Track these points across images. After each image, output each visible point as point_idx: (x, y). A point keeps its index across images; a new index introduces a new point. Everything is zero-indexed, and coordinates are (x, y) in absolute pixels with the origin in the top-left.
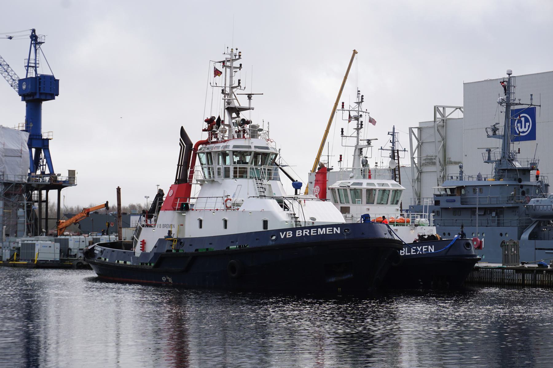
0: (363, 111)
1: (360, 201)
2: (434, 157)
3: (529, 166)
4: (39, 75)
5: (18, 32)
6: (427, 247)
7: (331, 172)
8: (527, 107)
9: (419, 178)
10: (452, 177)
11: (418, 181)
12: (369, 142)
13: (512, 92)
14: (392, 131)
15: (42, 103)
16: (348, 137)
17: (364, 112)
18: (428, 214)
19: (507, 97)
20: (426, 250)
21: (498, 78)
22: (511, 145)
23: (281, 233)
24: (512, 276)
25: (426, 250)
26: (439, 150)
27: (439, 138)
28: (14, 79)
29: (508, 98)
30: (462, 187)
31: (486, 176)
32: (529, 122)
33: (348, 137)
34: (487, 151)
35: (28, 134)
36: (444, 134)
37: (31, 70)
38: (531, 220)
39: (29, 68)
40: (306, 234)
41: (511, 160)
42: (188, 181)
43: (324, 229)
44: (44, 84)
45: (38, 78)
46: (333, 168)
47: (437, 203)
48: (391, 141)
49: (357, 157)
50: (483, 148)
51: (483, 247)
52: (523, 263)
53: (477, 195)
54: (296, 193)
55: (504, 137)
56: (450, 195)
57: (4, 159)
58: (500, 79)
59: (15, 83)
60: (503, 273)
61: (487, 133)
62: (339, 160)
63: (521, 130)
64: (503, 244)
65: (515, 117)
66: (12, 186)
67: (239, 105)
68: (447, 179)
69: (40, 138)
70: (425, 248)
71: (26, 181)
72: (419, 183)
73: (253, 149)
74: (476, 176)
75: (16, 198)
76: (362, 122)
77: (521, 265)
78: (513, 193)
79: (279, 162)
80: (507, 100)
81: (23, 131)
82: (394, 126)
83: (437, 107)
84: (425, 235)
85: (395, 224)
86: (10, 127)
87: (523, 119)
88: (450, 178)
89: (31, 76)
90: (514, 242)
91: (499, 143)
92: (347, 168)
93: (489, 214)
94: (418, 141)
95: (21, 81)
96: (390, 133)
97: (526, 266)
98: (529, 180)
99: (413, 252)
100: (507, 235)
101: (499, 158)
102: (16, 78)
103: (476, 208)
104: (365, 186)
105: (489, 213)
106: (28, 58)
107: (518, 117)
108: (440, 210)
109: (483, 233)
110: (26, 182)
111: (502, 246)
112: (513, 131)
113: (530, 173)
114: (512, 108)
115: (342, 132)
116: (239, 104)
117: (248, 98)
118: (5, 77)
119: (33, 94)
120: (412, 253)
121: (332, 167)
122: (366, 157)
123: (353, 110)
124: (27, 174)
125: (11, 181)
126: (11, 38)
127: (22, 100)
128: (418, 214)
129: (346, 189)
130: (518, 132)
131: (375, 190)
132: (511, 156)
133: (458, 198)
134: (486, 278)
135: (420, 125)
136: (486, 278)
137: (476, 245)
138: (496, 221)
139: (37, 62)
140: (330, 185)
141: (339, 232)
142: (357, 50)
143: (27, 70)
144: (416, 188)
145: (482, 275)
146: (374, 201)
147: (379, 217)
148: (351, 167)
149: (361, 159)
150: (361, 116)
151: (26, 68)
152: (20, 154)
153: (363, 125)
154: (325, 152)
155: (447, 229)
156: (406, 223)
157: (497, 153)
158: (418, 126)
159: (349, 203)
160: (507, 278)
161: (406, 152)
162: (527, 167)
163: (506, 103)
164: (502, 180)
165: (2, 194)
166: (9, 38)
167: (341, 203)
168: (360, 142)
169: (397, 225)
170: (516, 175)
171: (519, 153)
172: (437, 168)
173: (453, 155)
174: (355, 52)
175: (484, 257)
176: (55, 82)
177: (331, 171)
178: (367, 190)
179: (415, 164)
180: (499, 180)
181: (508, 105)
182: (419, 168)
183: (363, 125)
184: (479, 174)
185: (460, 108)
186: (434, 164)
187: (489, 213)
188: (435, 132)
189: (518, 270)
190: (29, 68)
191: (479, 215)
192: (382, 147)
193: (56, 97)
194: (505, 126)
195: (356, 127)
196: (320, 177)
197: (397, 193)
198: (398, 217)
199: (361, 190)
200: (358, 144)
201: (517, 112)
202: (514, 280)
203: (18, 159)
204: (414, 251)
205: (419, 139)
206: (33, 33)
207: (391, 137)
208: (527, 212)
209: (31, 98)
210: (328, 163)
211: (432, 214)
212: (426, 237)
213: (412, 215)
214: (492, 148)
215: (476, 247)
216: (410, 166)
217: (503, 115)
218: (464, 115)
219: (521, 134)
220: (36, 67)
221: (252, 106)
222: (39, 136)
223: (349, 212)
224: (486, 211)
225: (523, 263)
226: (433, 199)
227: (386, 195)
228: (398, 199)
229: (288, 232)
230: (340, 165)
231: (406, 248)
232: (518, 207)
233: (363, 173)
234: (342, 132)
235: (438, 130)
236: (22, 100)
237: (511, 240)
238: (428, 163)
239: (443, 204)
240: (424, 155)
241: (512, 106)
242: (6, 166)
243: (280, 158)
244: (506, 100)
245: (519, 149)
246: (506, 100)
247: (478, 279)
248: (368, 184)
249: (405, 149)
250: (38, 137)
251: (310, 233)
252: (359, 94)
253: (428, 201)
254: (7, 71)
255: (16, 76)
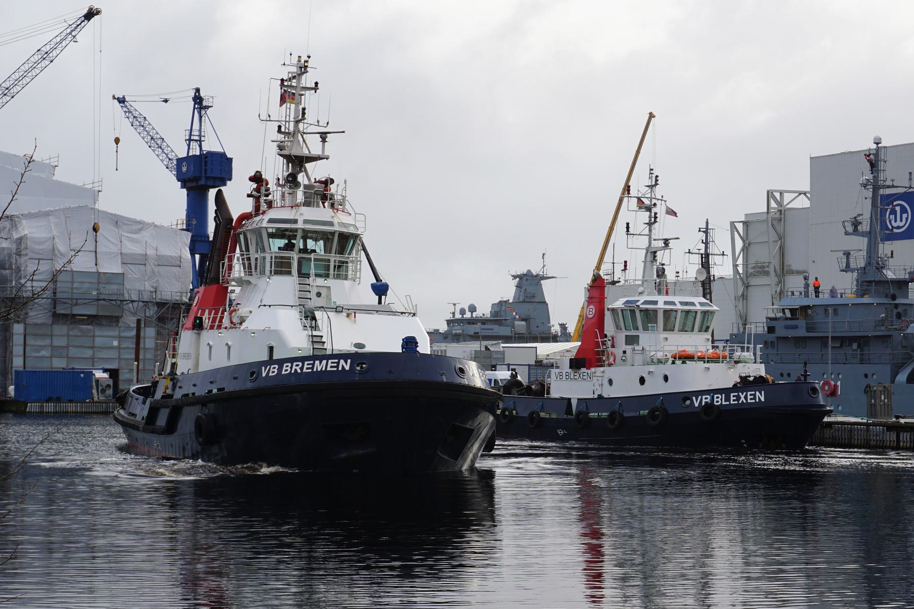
0: (657, 197)
1: (655, 326)
2: (767, 264)
3: (907, 276)
4: (205, 152)
5: (175, 93)
6: (754, 393)
7: (617, 286)
8: (902, 190)
9: (745, 294)
10: (793, 293)
11: (743, 299)
12: (666, 242)
13: (882, 169)
14: (705, 227)
15: (209, 191)
16: (636, 235)
17: (658, 199)
18: (752, 346)
19: (874, 177)
20: (752, 397)
21: (861, 149)
22: (881, 246)
23: (263, 368)
24: (881, 436)
25: (752, 397)
26: (774, 253)
27: (773, 236)
28: (170, 158)
29: (876, 178)
30: (808, 307)
31: (843, 291)
32: (907, 212)
33: (636, 235)
34: (844, 254)
35: (190, 234)
36: (782, 231)
37: (194, 145)
38: (910, 354)
39: (192, 142)
40: (296, 370)
41: (880, 268)
42: (221, 281)
43: (324, 362)
44: (221, 166)
45: (203, 157)
46: (621, 280)
47: (771, 330)
48: (703, 240)
49: (648, 264)
50: (839, 251)
51: (839, 394)
52: (897, 417)
53: (830, 319)
54: (380, 302)
55: (869, 234)
56: (790, 319)
57: (156, 269)
58: (864, 151)
59: (171, 163)
60: (868, 430)
61: (845, 229)
62: (623, 268)
63: (895, 225)
64: (868, 390)
65: (887, 206)
66: (169, 307)
67: (308, 153)
68: (785, 295)
69: (206, 239)
70: (751, 395)
71: (188, 301)
72: (745, 301)
73: (300, 225)
74: (829, 291)
75: (174, 323)
76: (656, 214)
77: (894, 419)
78: (883, 315)
79: (543, 272)
80: (874, 181)
81: (184, 230)
82: (707, 219)
83: (772, 193)
84: (750, 376)
85: (706, 360)
86: (165, 225)
87: (898, 209)
88: (790, 294)
89: (194, 153)
90: (885, 387)
91: (862, 243)
92: (635, 280)
93: (849, 346)
94: (744, 241)
95: (180, 161)
96: (701, 230)
97: (902, 421)
98: (907, 297)
99: (734, 400)
100: (875, 377)
101: (863, 265)
102: (173, 157)
103: (828, 337)
104: (661, 305)
105: (847, 345)
106: (189, 128)
107: (891, 206)
108: (775, 340)
109: (839, 374)
110: (187, 302)
111: (865, 392)
112: (884, 226)
113: (908, 286)
114: (881, 192)
115: (628, 228)
116: (309, 150)
117: (321, 140)
118: (158, 156)
119: (196, 179)
120: (732, 402)
121: (619, 278)
122: (663, 264)
123: (643, 196)
124: (189, 291)
125: (166, 300)
126: (166, 101)
127: (182, 188)
128: (739, 346)
129: (634, 310)
130: (890, 227)
131: (676, 311)
132: (880, 263)
133: (801, 323)
134: (842, 439)
135: (745, 218)
136: (842, 439)
137: (828, 390)
138: (859, 357)
139: (203, 134)
140: (609, 305)
141: (347, 368)
142: (655, 113)
143: (189, 146)
144: (741, 309)
145: (837, 434)
146: (674, 327)
147: (681, 350)
148: (641, 278)
149: (655, 267)
150: (655, 205)
151: (188, 142)
152: (178, 263)
153: (657, 217)
154: (608, 258)
155: (786, 368)
156: (721, 359)
157: (860, 257)
158: (743, 220)
159: (638, 330)
160: (874, 438)
161: (725, 256)
162: (903, 277)
163: (873, 185)
164: (867, 296)
165: (154, 319)
166: (163, 101)
167: (626, 330)
168: (653, 242)
169: (708, 362)
170: (888, 291)
171: (892, 257)
172: (772, 279)
173: (795, 261)
174: (651, 116)
175: (840, 408)
176: (226, 161)
177: (617, 284)
178: (664, 311)
179: (739, 274)
180: (862, 296)
181: (876, 188)
182: (745, 280)
183: (657, 217)
184: (833, 287)
185: (805, 194)
186: (767, 273)
187: (847, 345)
188: (768, 228)
189: (890, 428)
190: (192, 142)
191: (833, 348)
192: (689, 250)
193: (228, 183)
194: (871, 218)
195: (647, 222)
196: (596, 294)
197: (707, 316)
198: (708, 350)
199: (655, 311)
200: (650, 245)
201: (889, 199)
202: (884, 441)
203: (178, 268)
204: (735, 398)
205: (745, 239)
206: (197, 94)
207: (702, 236)
208: (904, 343)
209: (194, 184)
210: (613, 273)
211: (759, 346)
212: (751, 379)
213: (730, 347)
214: (852, 250)
215: (828, 393)
216: (732, 277)
217: (869, 202)
218: (811, 203)
219: (895, 231)
220: (200, 141)
221: (326, 153)
222: (205, 236)
223: (638, 344)
224: (843, 341)
225: (897, 417)
226: (765, 325)
227: (691, 318)
228: (708, 324)
229: (704, 397)
230: (624, 276)
231: (723, 395)
232: (890, 336)
233: (657, 287)
234: (628, 228)
235: (773, 225)
236: (182, 188)
237: (880, 383)
238: (758, 272)
239: (781, 332)
240: (752, 261)
241: (881, 190)
242: (160, 279)
243: (544, 267)
244: (872, 181)
245: (892, 252)
246: (872, 181)
247: (830, 440)
248: (666, 303)
249: (723, 252)
250: (203, 239)
251: (302, 369)
252: (653, 173)
253: (758, 326)
254: (161, 147)
255: (173, 154)
